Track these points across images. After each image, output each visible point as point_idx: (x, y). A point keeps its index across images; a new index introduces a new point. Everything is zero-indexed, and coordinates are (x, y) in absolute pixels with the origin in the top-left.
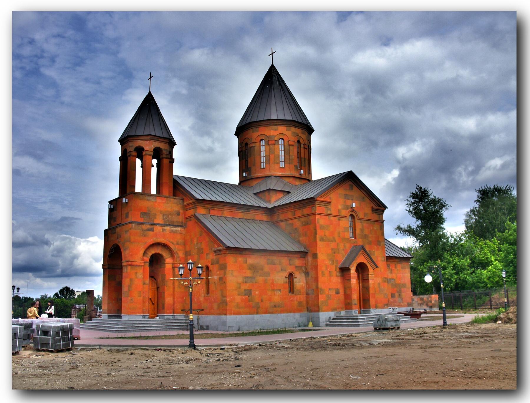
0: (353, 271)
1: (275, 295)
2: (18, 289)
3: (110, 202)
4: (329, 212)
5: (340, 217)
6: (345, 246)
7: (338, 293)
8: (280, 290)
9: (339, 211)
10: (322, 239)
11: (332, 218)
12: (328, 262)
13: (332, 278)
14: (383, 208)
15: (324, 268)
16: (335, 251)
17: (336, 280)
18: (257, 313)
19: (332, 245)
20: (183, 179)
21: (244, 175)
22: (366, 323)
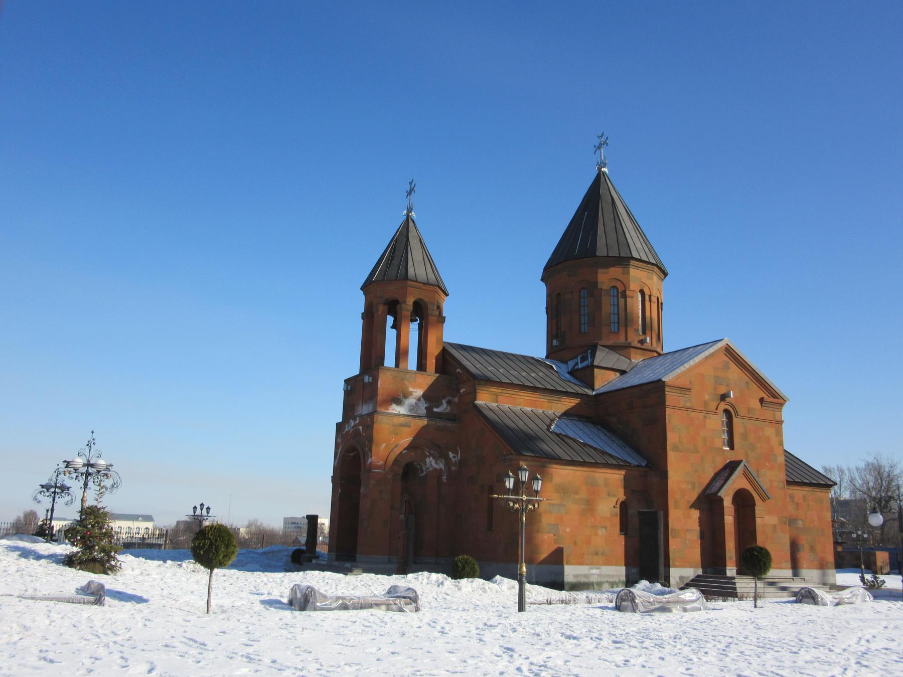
0: (728, 503)
1: (596, 534)
2: (208, 508)
4: (688, 405)
8: (605, 528)
9: (705, 403)
10: (676, 449)
22: (729, 519)
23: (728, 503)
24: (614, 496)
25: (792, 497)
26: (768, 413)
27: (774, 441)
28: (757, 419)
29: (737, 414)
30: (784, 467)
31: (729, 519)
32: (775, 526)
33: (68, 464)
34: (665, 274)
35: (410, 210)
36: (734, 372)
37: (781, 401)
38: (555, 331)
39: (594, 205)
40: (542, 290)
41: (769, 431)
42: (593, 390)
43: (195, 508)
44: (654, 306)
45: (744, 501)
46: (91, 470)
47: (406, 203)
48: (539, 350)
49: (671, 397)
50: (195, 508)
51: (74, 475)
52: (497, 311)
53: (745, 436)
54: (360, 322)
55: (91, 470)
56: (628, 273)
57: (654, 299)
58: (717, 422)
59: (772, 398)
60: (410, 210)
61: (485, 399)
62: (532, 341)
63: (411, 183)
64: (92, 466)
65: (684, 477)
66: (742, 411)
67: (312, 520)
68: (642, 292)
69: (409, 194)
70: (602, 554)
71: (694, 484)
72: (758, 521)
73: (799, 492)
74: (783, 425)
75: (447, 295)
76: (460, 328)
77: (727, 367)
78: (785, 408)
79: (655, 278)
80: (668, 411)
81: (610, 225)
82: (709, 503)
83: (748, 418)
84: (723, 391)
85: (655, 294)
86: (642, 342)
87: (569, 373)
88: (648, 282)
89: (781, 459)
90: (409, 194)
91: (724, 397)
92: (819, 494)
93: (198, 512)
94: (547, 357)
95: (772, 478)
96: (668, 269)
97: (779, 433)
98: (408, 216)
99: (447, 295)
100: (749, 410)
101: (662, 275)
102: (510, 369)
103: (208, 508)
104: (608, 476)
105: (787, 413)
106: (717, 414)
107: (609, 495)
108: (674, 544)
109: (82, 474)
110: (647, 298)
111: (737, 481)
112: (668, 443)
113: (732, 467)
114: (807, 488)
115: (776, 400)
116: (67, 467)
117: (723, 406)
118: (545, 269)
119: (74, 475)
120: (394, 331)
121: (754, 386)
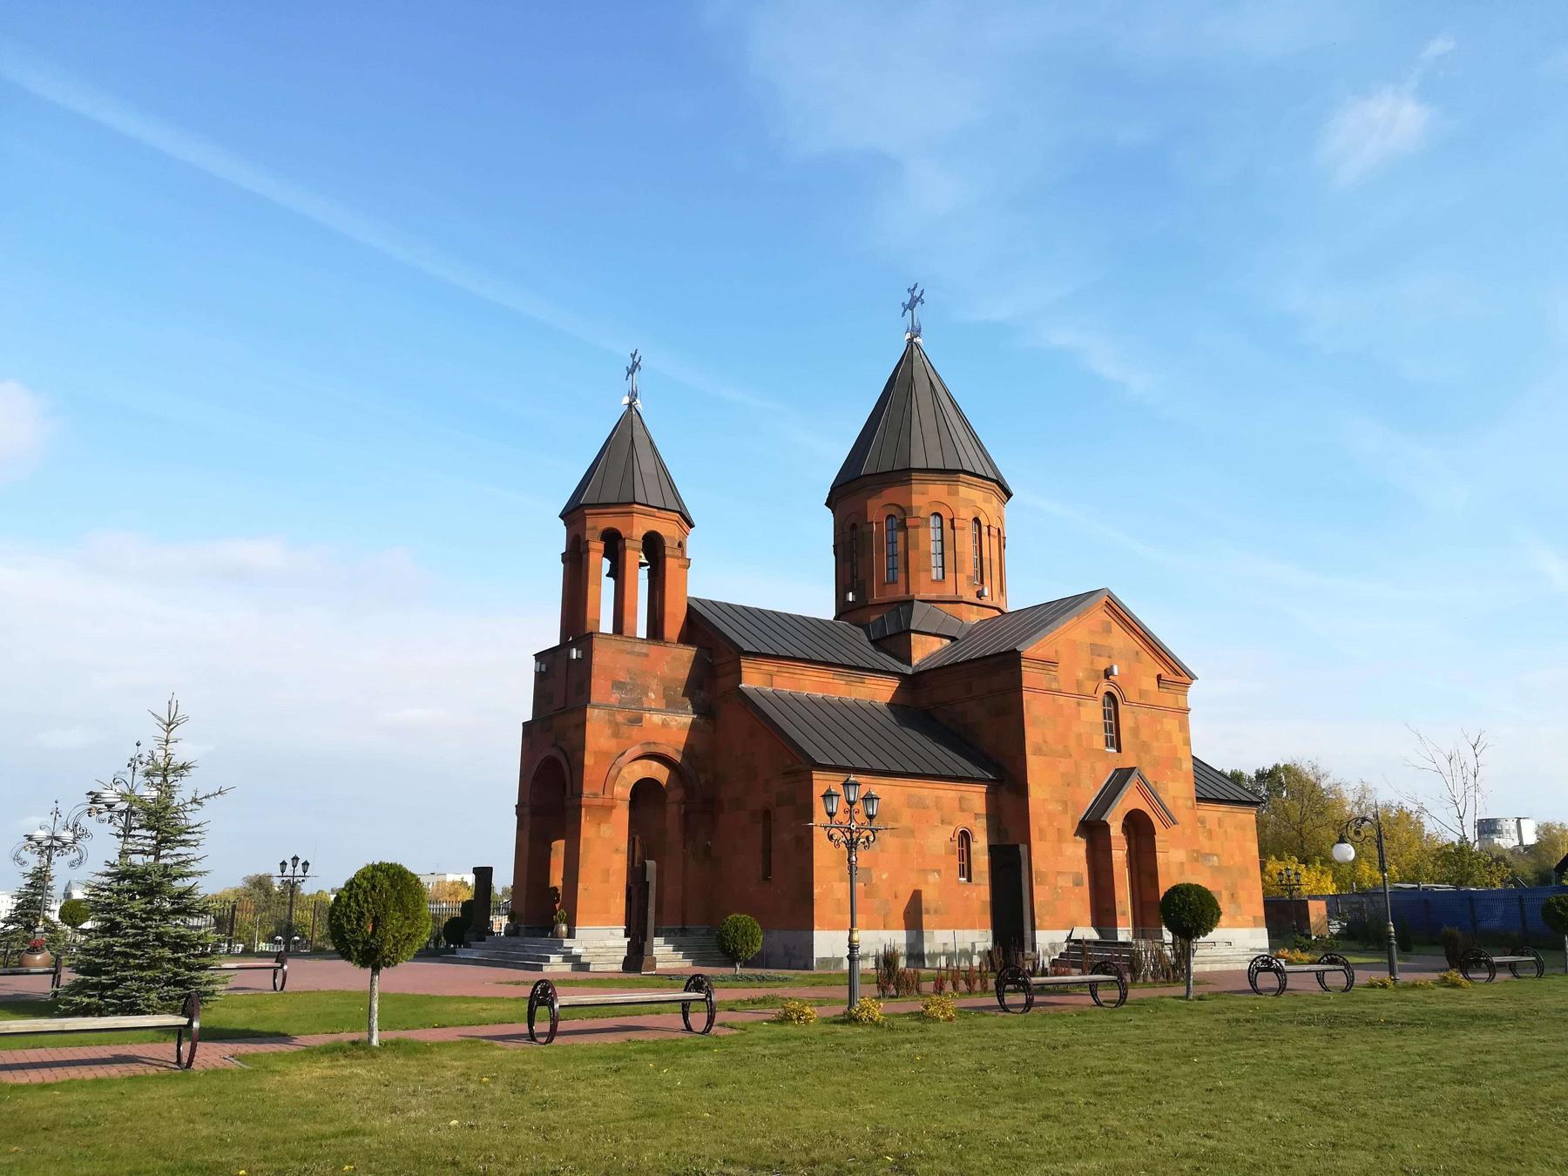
0: (1116, 830)
1: (926, 882)
2: (306, 864)
3: (539, 657)
4: (1054, 686)
5: (1081, 696)
6: (1093, 769)
7: (1078, 884)
8: (939, 872)
9: (1079, 684)
10: (1038, 751)
11: (1062, 700)
12: (1054, 807)
13: (1064, 845)
14: (1186, 679)
15: (1044, 823)
16: (1071, 781)
17: (1077, 850)
18: (885, 928)
19: (1064, 765)
20: (744, 613)
21: (850, 597)
22: (1119, 854)
23: (1116, 830)
24: (950, 823)
25: (1202, 821)
26: (1167, 698)
27: (1177, 738)
28: (1152, 706)
29: (1124, 699)
30: (1192, 779)
31: (1119, 854)
32: (1182, 864)
33: (95, 798)
34: (1009, 495)
35: (633, 395)
36: (1119, 638)
37: (1186, 679)
38: (845, 579)
39: (905, 394)
40: (828, 517)
41: (1170, 724)
42: (910, 664)
43: (284, 864)
44: (995, 542)
45: (1138, 825)
46: (55, 843)
47: (627, 386)
48: (825, 609)
49: (1029, 675)
50: (284, 864)
51: (106, 815)
52: (765, 556)
53: (1135, 731)
54: (560, 568)
55: (55, 843)
56: (956, 493)
57: (994, 532)
58: (1093, 712)
59: (1176, 675)
60: (633, 395)
61: (754, 678)
62: (814, 596)
63: (633, 356)
64: (57, 839)
65: (1056, 791)
66: (1131, 695)
67: (484, 875)
68: (976, 520)
69: (631, 371)
70: (936, 912)
71: (1065, 804)
72: (1160, 857)
73: (1212, 812)
74: (1190, 715)
75: (691, 526)
76: (714, 575)
77: (1108, 630)
78: (1194, 689)
79: (995, 500)
80: (1026, 696)
81: (929, 424)
82: (1092, 829)
83: (1140, 705)
84: (1103, 664)
85: (995, 524)
86: (980, 595)
87: (872, 642)
88: (986, 507)
89: (1188, 766)
90: (631, 371)
91: (1108, 673)
92: (1240, 816)
93: (289, 870)
94: (837, 618)
95: (1178, 791)
96: (1012, 489)
97: (1184, 727)
98: (630, 405)
99: (691, 526)
100: (1142, 693)
101: (1004, 497)
102: (787, 638)
103: (306, 864)
104: (940, 793)
105: (1195, 695)
106: (1095, 699)
107: (942, 822)
108: (1041, 894)
109: (121, 813)
110: (985, 530)
111: (1130, 800)
112: (1027, 742)
113: (1121, 777)
114: (1223, 808)
115: (1178, 679)
116: (94, 802)
117: (1105, 687)
118: (833, 488)
119: (106, 815)
120: (611, 581)
121: (1147, 657)
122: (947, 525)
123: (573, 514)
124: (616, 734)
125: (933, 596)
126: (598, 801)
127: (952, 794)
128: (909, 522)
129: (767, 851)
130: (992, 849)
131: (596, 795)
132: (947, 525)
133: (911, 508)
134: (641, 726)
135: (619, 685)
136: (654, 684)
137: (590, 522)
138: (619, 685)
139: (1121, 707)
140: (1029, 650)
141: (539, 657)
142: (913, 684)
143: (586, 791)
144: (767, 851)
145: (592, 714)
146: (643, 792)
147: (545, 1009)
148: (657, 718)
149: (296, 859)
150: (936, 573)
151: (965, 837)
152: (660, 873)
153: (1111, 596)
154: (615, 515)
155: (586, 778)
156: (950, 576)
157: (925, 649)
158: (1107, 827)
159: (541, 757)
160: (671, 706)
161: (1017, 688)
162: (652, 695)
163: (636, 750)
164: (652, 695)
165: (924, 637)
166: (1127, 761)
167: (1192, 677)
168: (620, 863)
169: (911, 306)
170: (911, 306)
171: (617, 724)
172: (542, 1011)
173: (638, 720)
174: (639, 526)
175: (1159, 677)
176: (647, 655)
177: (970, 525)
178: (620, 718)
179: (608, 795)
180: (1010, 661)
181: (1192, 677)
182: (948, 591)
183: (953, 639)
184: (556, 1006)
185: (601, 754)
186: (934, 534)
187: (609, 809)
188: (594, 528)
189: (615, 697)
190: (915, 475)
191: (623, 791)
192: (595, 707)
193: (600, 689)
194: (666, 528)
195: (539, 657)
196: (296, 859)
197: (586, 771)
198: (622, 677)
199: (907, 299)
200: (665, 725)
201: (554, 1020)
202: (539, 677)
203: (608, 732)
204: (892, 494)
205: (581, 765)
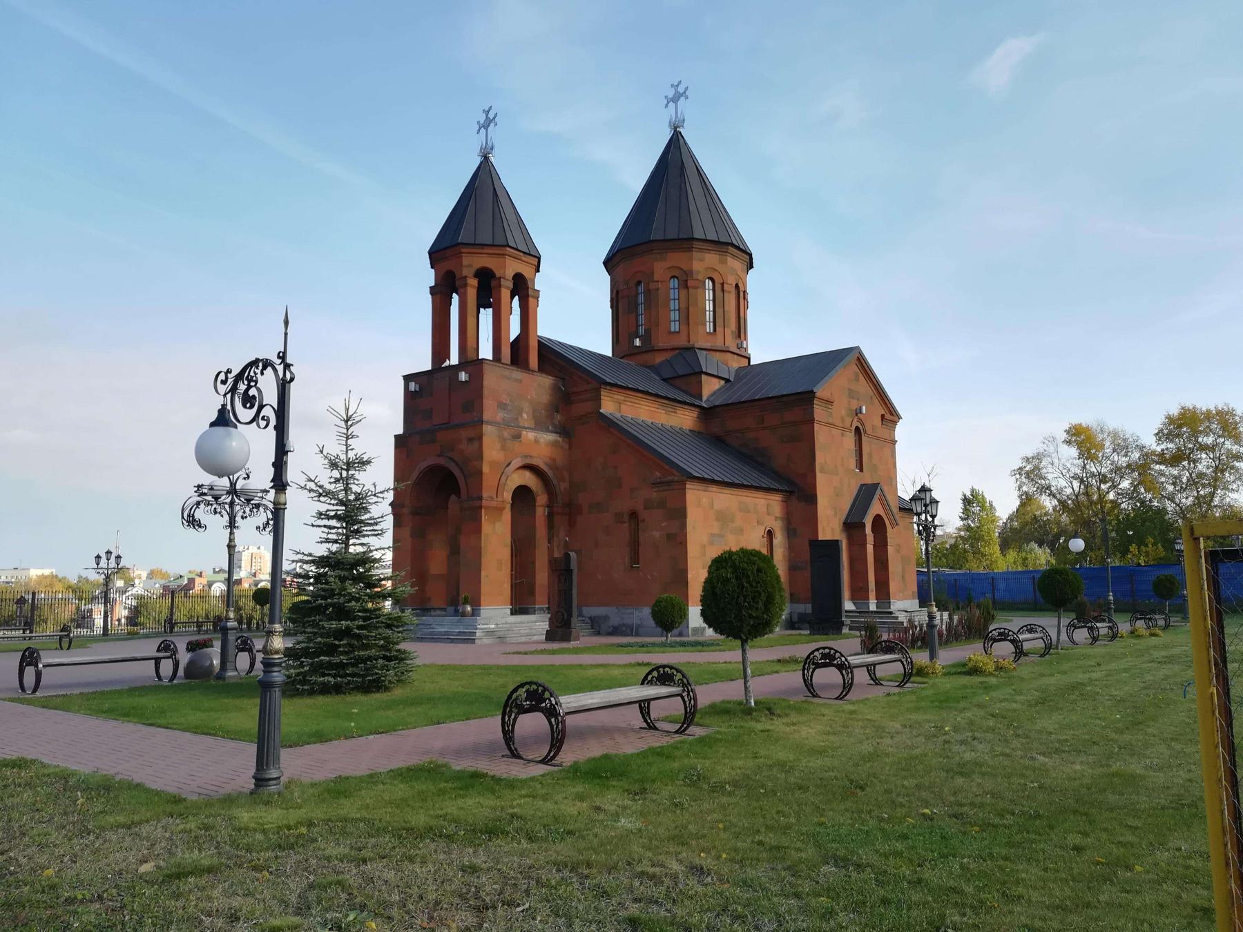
2: (118, 557)
11: (834, 431)
43: (98, 557)
45: (878, 522)
49: (819, 412)
56: (725, 262)
66: (869, 431)
77: (857, 379)
84: (854, 406)
104: (748, 500)
117: (856, 423)
122: (718, 287)
123: (437, 254)
124: (503, 448)
125: (707, 345)
126: (494, 504)
127: (762, 502)
128: (690, 283)
129: (635, 545)
130: (865, 544)
131: (492, 499)
132: (718, 287)
133: (691, 272)
134: (515, 440)
135: (502, 406)
136: (526, 406)
137: (466, 260)
138: (502, 406)
139: (864, 438)
140: (821, 391)
141: (408, 378)
142: (707, 413)
143: (485, 495)
144: (635, 545)
145: (488, 430)
146: (522, 493)
147: (32, 668)
148: (531, 435)
149: (109, 553)
150: (709, 327)
151: (770, 534)
152: (579, 563)
153: (861, 353)
154: (477, 252)
155: (484, 484)
156: (719, 329)
157: (710, 387)
158: (864, 525)
159: (423, 465)
160: (539, 426)
161: (811, 421)
162: (525, 416)
163: (517, 462)
164: (525, 416)
165: (709, 378)
166: (868, 479)
167: (900, 418)
168: (505, 554)
169: (675, 99)
170: (675, 99)
171: (505, 440)
172: (30, 672)
173: (517, 437)
174: (511, 268)
175: (883, 416)
176: (520, 381)
177: (733, 290)
178: (506, 434)
179: (500, 499)
180: (807, 398)
181: (900, 418)
182: (719, 343)
183: (727, 381)
184: (40, 666)
185: (493, 464)
186: (709, 295)
187: (500, 510)
188: (470, 266)
189: (501, 415)
190: (696, 244)
191: (508, 496)
192: (488, 423)
193: (490, 411)
194: (526, 271)
195: (408, 378)
196: (109, 553)
197: (484, 478)
198: (505, 399)
199: (671, 93)
200: (537, 441)
201: (39, 675)
202: (410, 397)
203: (498, 446)
204: (676, 259)
205: (480, 473)
